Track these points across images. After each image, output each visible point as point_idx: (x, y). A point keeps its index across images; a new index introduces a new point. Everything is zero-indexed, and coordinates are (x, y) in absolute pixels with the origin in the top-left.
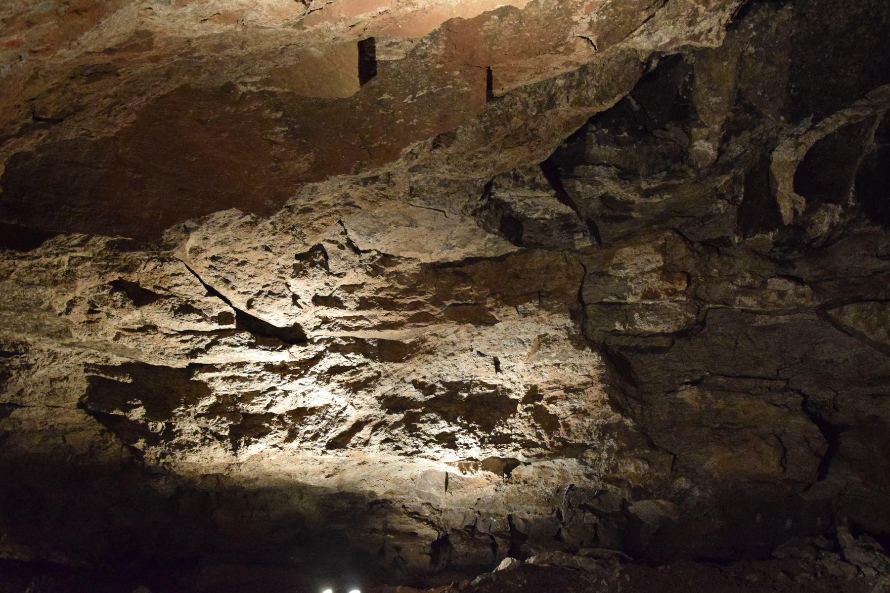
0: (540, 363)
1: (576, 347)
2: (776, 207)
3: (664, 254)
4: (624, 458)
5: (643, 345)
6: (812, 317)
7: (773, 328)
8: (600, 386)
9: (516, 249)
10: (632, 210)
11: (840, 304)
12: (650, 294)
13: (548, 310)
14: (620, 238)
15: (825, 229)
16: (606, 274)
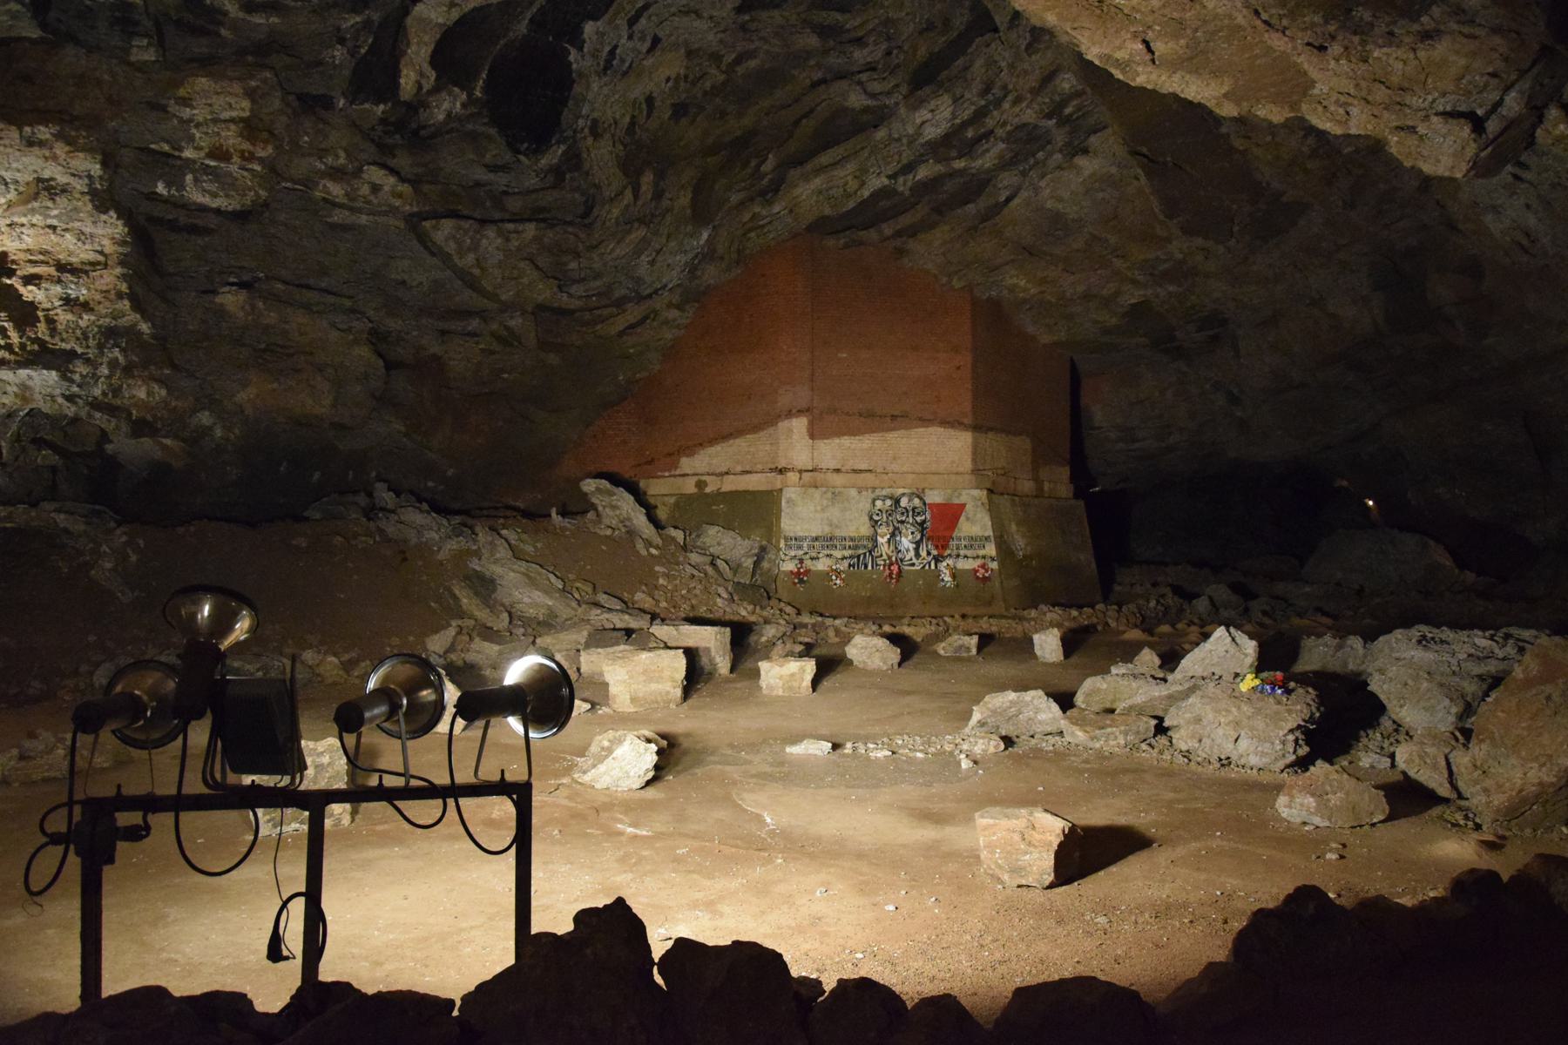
0: (24, 220)
1: (96, 208)
2: (395, 74)
3: (253, 101)
4: (133, 377)
5: (183, 220)
6: (397, 223)
7: (345, 228)
8: (118, 271)
9: (35, 33)
10: (221, 24)
11: (437, 216)
12: (220, 154)
13: (69, 144)
14: (192, 60)
15: (441, 117)
16: (164, 109)
